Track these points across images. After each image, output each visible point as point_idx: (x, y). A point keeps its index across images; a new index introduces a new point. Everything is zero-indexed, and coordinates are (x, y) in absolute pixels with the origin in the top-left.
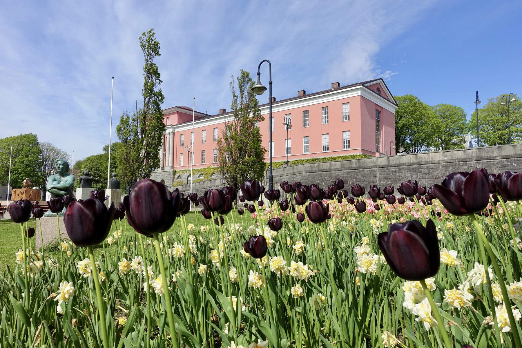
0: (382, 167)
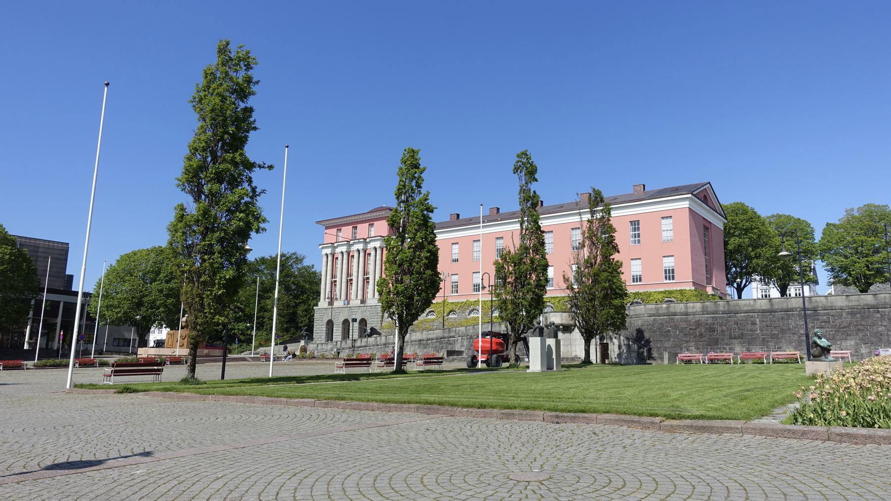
0: (763, 311)
